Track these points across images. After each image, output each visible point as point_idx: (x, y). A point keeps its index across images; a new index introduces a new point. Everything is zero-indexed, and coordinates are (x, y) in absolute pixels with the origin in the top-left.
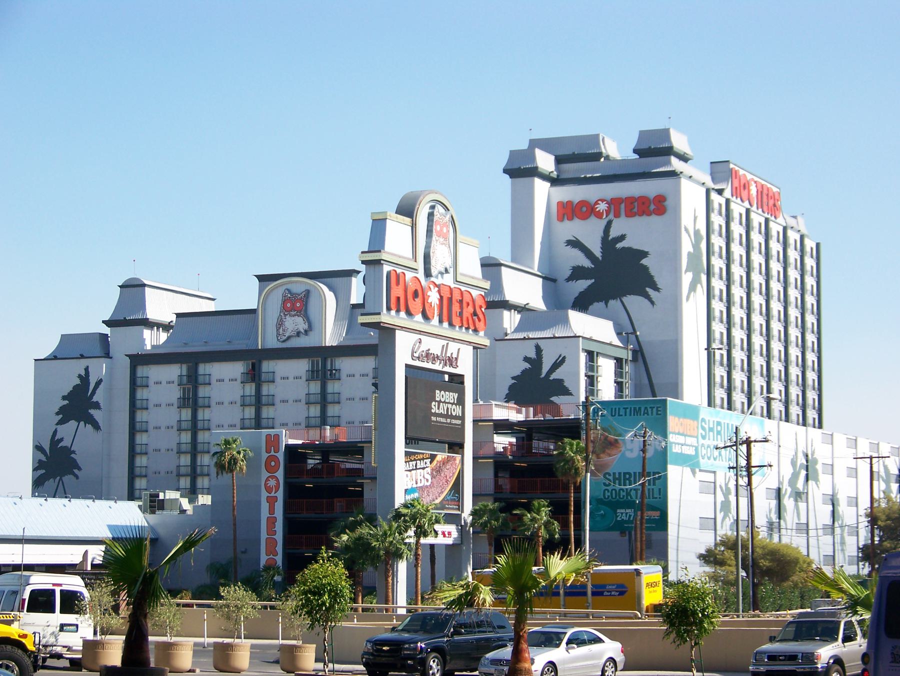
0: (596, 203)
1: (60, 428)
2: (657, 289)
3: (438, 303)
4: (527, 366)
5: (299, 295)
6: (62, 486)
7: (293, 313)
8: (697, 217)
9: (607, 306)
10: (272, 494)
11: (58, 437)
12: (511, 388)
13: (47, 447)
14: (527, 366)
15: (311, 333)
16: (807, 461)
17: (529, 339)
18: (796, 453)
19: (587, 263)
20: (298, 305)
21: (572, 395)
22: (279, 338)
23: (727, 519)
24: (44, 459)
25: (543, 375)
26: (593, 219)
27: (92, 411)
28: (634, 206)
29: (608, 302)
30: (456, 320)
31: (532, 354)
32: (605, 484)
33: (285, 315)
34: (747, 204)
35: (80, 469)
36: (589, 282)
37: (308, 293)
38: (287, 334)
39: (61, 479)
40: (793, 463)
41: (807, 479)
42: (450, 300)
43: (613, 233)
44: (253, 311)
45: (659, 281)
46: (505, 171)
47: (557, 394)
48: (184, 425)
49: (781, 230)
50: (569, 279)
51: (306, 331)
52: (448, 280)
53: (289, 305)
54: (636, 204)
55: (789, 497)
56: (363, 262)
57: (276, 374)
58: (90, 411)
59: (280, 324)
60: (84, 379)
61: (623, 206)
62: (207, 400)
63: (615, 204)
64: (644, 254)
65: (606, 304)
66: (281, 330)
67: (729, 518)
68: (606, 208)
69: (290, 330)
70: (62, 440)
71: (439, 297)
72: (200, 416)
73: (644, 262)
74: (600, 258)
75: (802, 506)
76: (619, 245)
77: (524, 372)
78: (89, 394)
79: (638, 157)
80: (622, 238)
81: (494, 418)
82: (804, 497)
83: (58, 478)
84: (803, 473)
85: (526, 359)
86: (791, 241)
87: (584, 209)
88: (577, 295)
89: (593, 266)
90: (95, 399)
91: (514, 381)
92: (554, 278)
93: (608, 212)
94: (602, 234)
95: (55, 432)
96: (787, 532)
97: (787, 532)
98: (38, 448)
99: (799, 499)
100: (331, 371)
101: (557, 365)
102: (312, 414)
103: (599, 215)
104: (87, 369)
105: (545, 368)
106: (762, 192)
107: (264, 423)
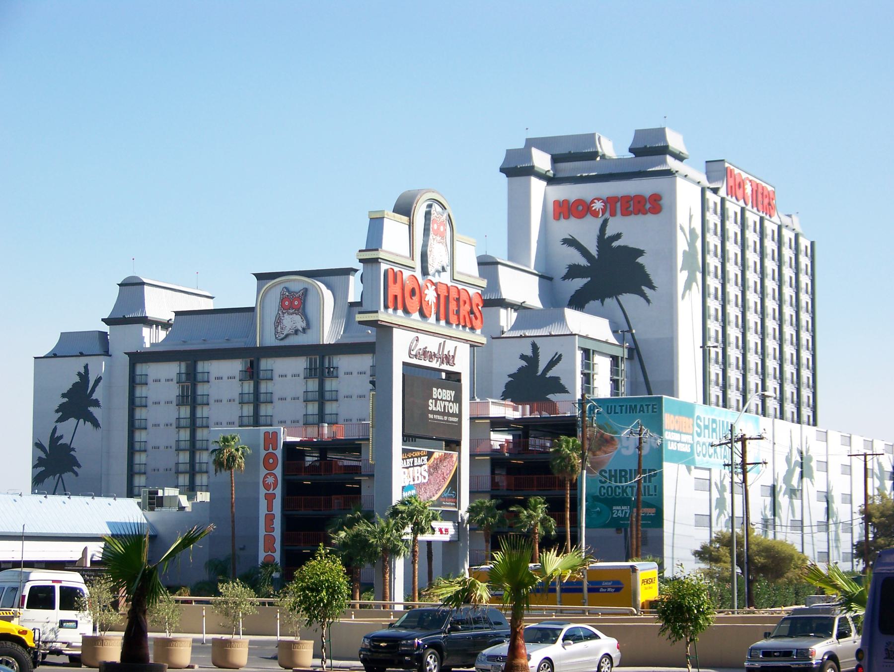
0: (592, 202)
1: (60, 425)
2: (652, 287)
3: (435, 301)
4: (524, 363)
5: (297, 293)
6: (62, 484)
7: (291, 311)
8: (692, 215)
9: (603, 304)
10: (271, 491)
11: (57, 434)
12: (508, 385)
13: (46, 444)
14: (524, 363)
15: (309, 331)
16: (802, 458)
17: (526, 337)
18: (791, 451)
19: (583, 262)
20: (296, 303)
21: (568, 392)
22: (277, 336)
23: (722, 516)
24: (43, 456)
25: (539, 373)
26: (589, 218)
27: (91, 409)
28: (630, 204)
29: (604, 300)
30: (453, 318)
31: (529, 352)
32: (601, 481)
33: (283, 313)
34: (742, 203)
35: (79, 466)
36: (585, 280)
37: (306, 291)
38: (285, 333)
39: (60, 476)
40: (788, 460)
41: (802, 476)
42: (447, 298)
43: (609, 232)
44: (251, 310)
45: (655, 279)
46: (502, 170)
47: (554, 392)
48: (183, 423)
49: (776, 228)
50: (565, 277)
51: (304, 329)
52: (445, 278)
53: (287, 303)
54: (632, 203)
55: (784, 494)
56: (361, 261)
57: (274, 372)
58: (89, 409)
59: (278, 322)
60: (84, 377)
61: (619, 205)
62: (205, 398)
63: (611, 203)
64: (640, 253)
65: (602, 302)
66: (279, 328)
67: (724, 515)
68: (602, 207)
69: (288, 329)
70: (61, 437)
71: (436, 295)
72: (199, 413)
73: (640, 260)
74: (596, 257)
75: (797, 503)
76: (615, 244)
77: (521, 370)
78: (89, 391)
79: (634, 156)
80: (618, 236)
81: (491, 416)
82: (798, 494)
83: (58, 475)
84: (798, 470)
85: (523, 357)
86: (786, 240)
87: (580, 208)
88: (573, 293)
89: (589, 265)
90: (94, 397)
91: (510, 379)
92: (550, 276)
93: (604, 211)
94: (598, 232)
95: (55, 430)
96: (782, 529)
97: (782, 529)
98: (38, 445)
99: (793, 496)
100: (329, 368)
101: (553, 363)
102: (310, 412)
103: (595, 214)
104: (86, 367)
105: (542, 366)
106: (757, 191)
107: (262, 420)
